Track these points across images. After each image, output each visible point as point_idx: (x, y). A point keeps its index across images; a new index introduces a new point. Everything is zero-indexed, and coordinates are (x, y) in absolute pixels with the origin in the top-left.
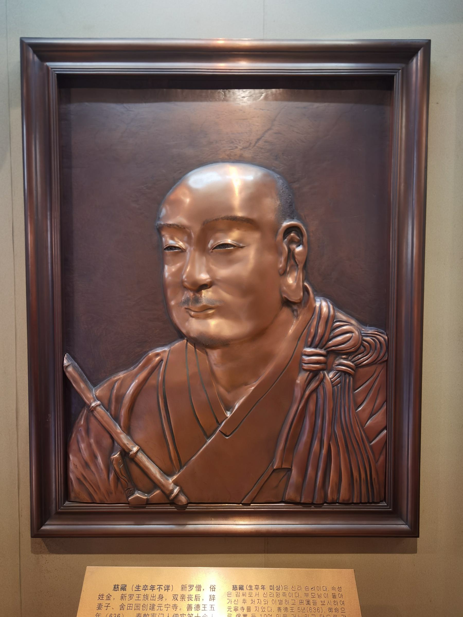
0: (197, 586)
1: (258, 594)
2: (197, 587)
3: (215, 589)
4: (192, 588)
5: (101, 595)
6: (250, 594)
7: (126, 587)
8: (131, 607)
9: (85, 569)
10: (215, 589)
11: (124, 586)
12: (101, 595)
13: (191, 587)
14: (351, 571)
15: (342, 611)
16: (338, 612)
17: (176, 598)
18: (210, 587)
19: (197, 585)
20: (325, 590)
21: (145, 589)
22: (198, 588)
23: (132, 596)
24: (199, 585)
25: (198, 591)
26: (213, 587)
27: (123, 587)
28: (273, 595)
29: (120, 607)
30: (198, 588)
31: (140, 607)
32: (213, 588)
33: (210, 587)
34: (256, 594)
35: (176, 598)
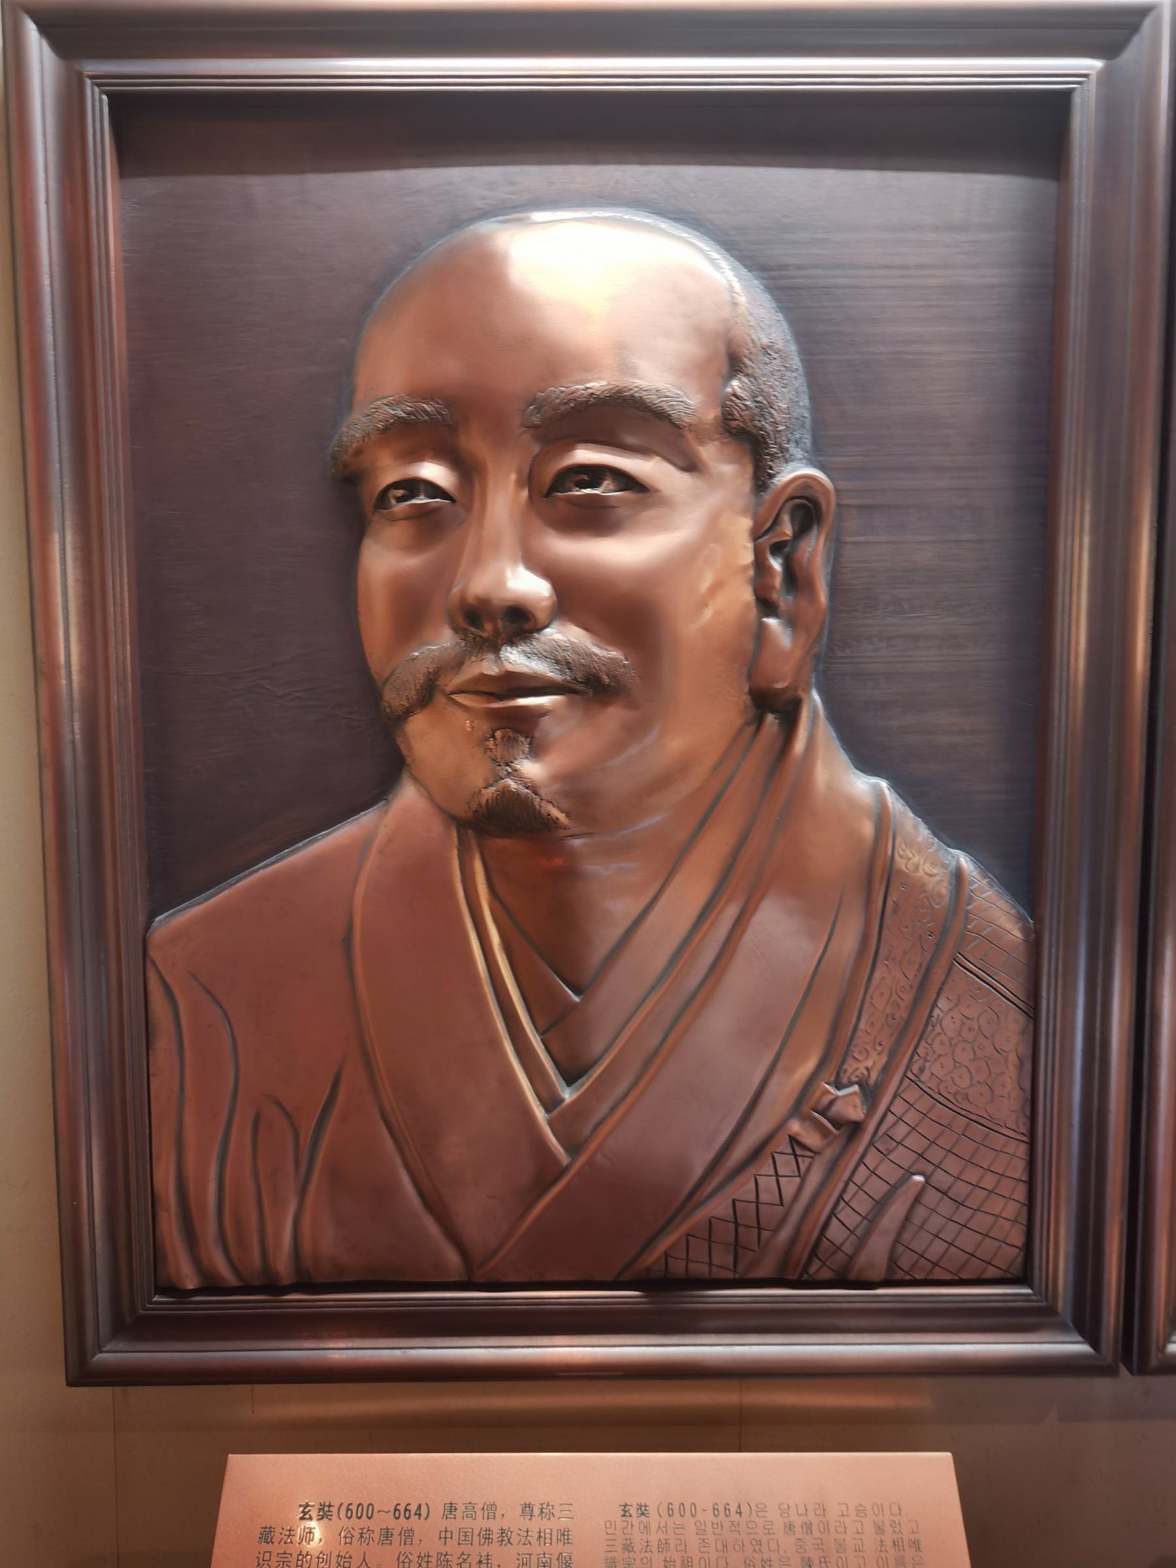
0: (403, 1532)
1: (666, 1527)
2: (403, 1535)
3: (351, 1538)
4: (391, 1540)
5: (422, 1555)
6: (769, 1527)
7: (274, 1532)
8: (442, 1536)
9: (226, 1462)
10: (351, 1538)
11: (267, 1530)
12: (422, 1555)
13: (562, 1537)
14: (232, 1457)
15: (750, 1531)
16: (491, 1543)
17: (509, 1540)
18: (397, 1557)
19: (485, 1503)
20: (775, 1550)
21: (704, 1543)
22: (405, 1536)
23: (564, 1539)
24: (492, 1503)
25: (488, 1518)
26: (405, 1559)
27: (264, 1532)
28: (824, 1510)
29: (708, 1544)
30: (405, 1536)
31: (474, 1538)
32: (407, 1560)
33: (745, 1562)
34: (659, 1527)
35: (509, 1540)
